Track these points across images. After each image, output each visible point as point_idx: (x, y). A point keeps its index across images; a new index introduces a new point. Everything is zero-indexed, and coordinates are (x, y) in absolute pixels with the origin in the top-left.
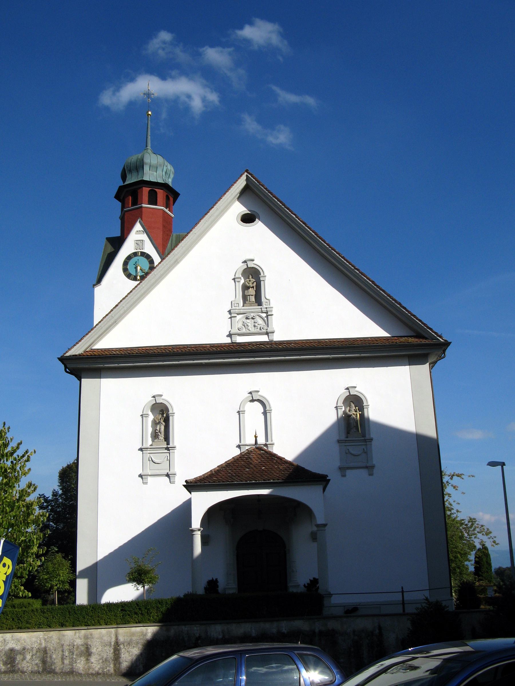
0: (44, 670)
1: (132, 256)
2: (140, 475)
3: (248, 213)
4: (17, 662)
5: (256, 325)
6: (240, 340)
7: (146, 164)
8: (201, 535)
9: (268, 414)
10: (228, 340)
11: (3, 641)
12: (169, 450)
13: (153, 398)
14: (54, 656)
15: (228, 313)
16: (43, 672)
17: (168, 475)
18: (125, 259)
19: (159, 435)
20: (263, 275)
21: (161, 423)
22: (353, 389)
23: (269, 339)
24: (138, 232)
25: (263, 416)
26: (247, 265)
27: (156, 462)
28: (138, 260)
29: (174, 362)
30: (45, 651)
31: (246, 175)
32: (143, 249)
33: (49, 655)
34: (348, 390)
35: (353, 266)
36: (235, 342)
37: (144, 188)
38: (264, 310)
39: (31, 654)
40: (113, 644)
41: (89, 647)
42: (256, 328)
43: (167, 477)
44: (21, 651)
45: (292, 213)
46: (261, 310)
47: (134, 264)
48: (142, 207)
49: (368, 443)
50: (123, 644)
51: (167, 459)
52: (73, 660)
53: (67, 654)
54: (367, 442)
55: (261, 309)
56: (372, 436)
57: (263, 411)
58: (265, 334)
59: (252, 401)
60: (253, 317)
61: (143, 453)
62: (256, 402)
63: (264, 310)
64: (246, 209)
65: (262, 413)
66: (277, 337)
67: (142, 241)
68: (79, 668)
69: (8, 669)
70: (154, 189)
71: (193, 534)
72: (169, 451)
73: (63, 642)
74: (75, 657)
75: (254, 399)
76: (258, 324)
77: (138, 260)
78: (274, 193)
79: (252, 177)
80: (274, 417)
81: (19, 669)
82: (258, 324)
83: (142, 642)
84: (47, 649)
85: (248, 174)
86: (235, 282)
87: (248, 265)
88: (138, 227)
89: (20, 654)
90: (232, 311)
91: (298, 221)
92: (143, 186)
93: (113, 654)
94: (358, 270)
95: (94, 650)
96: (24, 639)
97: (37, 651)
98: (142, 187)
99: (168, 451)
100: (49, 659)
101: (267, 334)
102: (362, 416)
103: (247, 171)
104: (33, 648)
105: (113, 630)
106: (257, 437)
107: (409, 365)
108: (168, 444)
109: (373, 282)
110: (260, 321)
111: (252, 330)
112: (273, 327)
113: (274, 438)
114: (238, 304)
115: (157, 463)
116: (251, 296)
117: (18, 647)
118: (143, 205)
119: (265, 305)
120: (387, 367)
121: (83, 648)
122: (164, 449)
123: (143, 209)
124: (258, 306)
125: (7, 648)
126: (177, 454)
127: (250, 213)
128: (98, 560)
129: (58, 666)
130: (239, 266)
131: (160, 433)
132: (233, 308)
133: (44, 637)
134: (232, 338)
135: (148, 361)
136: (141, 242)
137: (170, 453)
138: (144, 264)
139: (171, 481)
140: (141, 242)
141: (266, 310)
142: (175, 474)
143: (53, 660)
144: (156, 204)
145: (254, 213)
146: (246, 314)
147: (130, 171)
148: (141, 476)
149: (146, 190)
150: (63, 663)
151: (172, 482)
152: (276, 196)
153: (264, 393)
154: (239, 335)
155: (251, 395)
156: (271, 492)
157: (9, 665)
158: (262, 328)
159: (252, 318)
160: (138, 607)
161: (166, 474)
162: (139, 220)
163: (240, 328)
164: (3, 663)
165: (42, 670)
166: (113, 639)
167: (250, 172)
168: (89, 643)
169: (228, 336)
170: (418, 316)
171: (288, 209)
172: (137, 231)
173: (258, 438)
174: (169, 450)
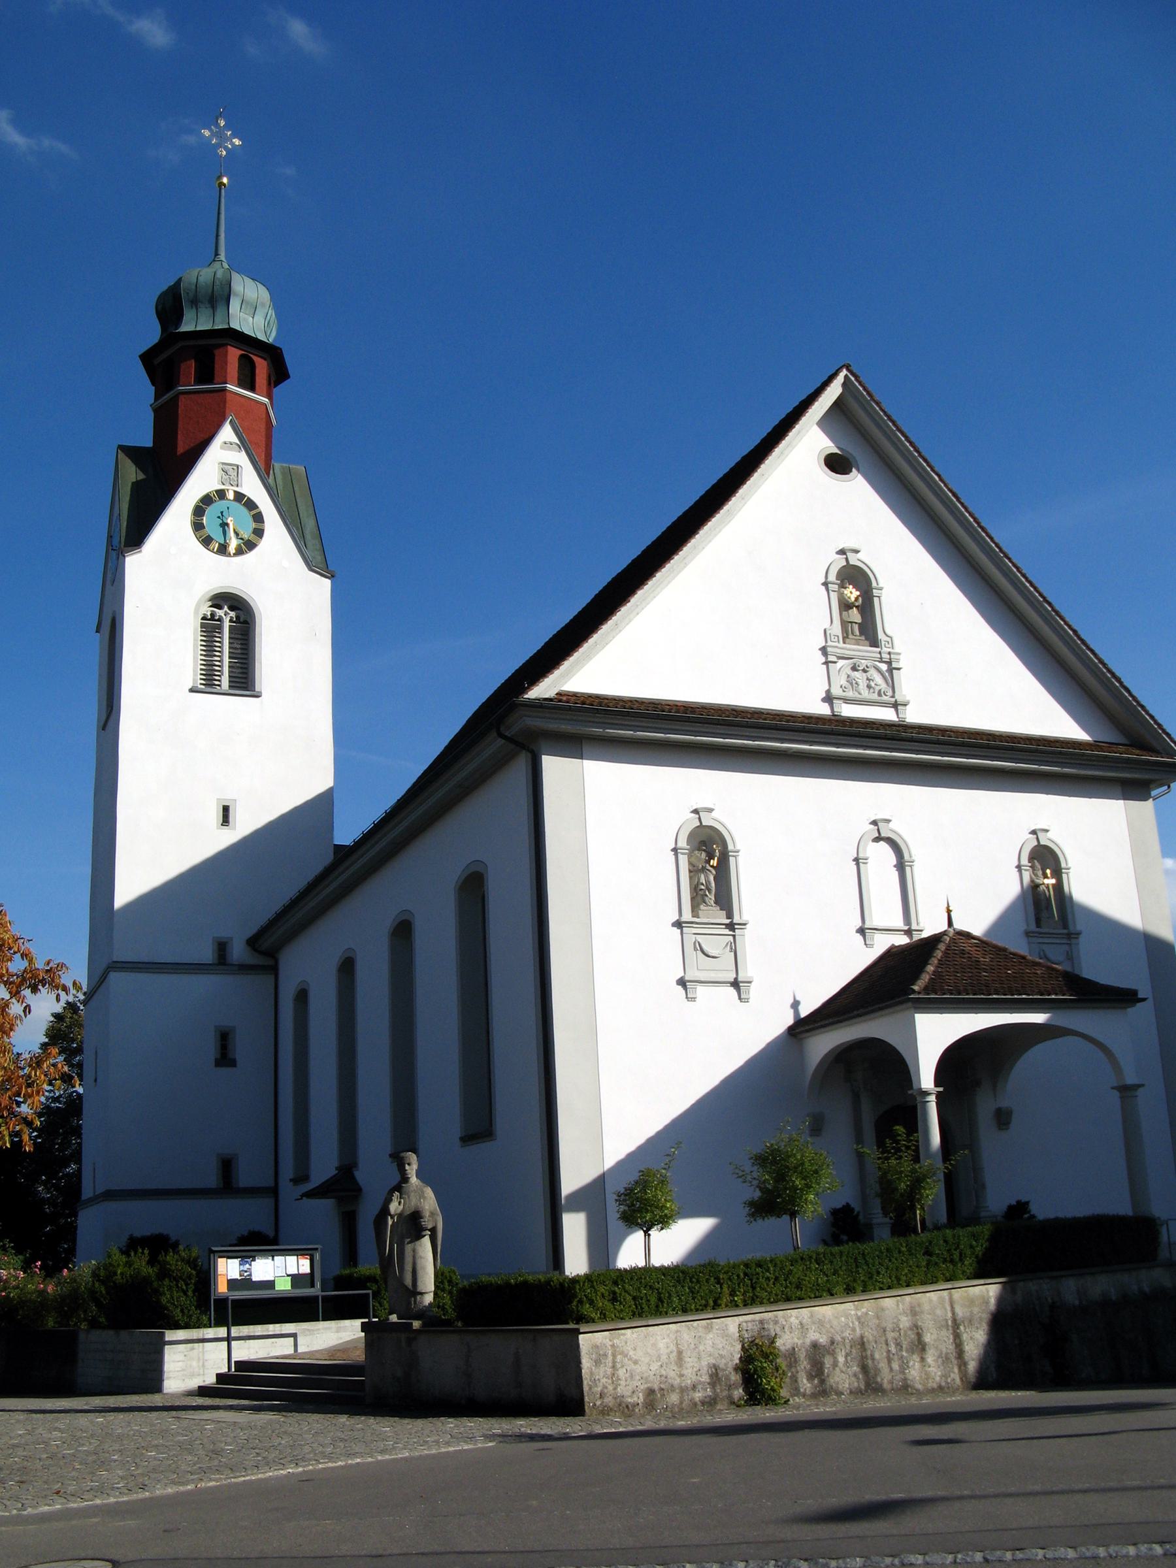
0: (868, 1384)
1: (214, 498)
2: (679, 979)
3: (836, 453)
4: (826, 1371)
5: (872, 684)
6: (848, 711)
7: (237, 295)
8: (937, 1103)
9: (908, 869)
10: (824, 710)
11: (799, 1327)
12: (733, 930)
13: (693, 815)
14: (877, 1356)
15: (820, 652)
16: (866, 1391)
17: (736, 984)
18: (197, 502)
19: (707, 895)
20: (876, 585)
21: (708, 870)
22: (1044, 834)
23: (898, 717)
24: (227, 445)
25: (897, 872)
26: (847, 559)
27: (710, 954)
28: (228, 508)
29: (745, 742)
30: (862, 1343)
31: (844, 374)
32: (237, 486)
33: (869, 1353)
34: (1035, 836)
35: (1041, 595)
36: (839, 714)
37: (229, 347)
38: (886, 657)
39: (843, 1353)
40: (950, 1323)
41: (920, 1331)
42: (872, 690)
43: (732, 988)
44: (829, 1348)
45: (933, 470)
46: (879, 656)
47: (219, 517)
48: (224, 390)
49: (1073, 941)
50: (963, 1322)
51: (732, 949)
52: (903, 1362)
53: (893, 1349)
54: (1072, 940)
55: (880, 653)
56: (1079, 927)
57: (895, 862)
58: (891, 705)
59: (878, 839)
60: (866, 668)
61: (684, 932)
62: (882, 842)
63: (886, 657)
64: (832, 444)
65: (895, 866)
66: (913, 716)
67: (235, 468)
68: (915, 1378)
69: (816, 1388)
70: (251, 356)
71: (927, 1100)
72: (734, 932)
73: (884, 1324)
74: (904, 1354)
75: (883, 835)
76: (876, 684)
77: (228, 508)
78: (899, 423)
79: (857, 380)
80: (919, 874)
81: (831, 1387)
82: (876, 684)
83: (986, 1317)
84: (865, 1340)
85: (848, 374)
86: (827, 590)
87: (849, 559)
88: (226, 433)
89: (829, 1353)
90: (829, 649)
91: (944, 488)
92: (230, 343)
93: (954, 1345)
94: (1050, 604)
95: (928, 1338)
96: (830, 1321)
97: (851, 1347)
98: (227, 345)
99: (730, 931)
100: (870, 1362)
101: (895, 705)
102: (1059, 887)
103: (848, 368)
104: (843, 1339)
105: (945, 1293)
106: (951, 911)
107: (1124, 799)
108: (730, 915)
109: (1075, 632)
110: (878, 679)
111: (865, 694)
112: (904, 693)
113: (921, 919)
114: (836, 637)
115: (713, 957)
116: (854, 624)
117: (823, 1340)
118: (228, 385)
119: (885, 647)
120: (1070, 796)
121: (913, 1334)
122: (724, 927)
123: (229, 397)
124: (871, 646)
125: (808, 1342)
126: (748, 939)
127: (840, 455)
128: (605, 1169)
129: (885, 1378)
130: (828, 561)
131: (709, 892)
132: (830, 643)
133: (857, 1314)
134: (833, 705)
135: (695, 731)
136: (233, 469)
137: (737, 937)
138: (239, 521)
139: (742, 997)
140: (233, 469)
141: (888, 656)
142: (750, 982)
143: (876, 1363)
144: (252, 388)
145: (848, 456)
146: (852, 660)
147: (195, 302)
148: (682, 982)
149: (234, 354)
150: (891, 1370)
151: (745, 999)
152: (903, 429)
153: (899, 828)
154: (847, 701)
155: (876, 827)
156: (1048, 1020)
157: (816, 1379)
158: (884, 692)
159: (865, 671)
160: (449, 1286)
161: (733, 980)
162: (231, 417)
163: (845, 687)
164: (807, 1376)
165: (865, 1387)
166: (950, 1315)
167: (854, 371)
168: (920, 1324)
169: (824, 700)
170: (1148, 708)
171: (925, 460)
172: (226, 443)
173: (952, 914)
174: (733, 930)
